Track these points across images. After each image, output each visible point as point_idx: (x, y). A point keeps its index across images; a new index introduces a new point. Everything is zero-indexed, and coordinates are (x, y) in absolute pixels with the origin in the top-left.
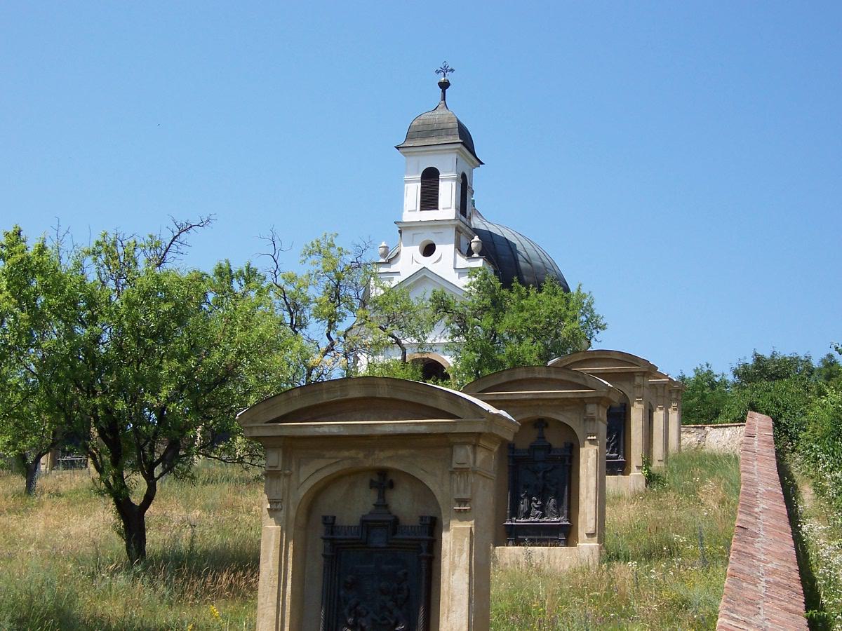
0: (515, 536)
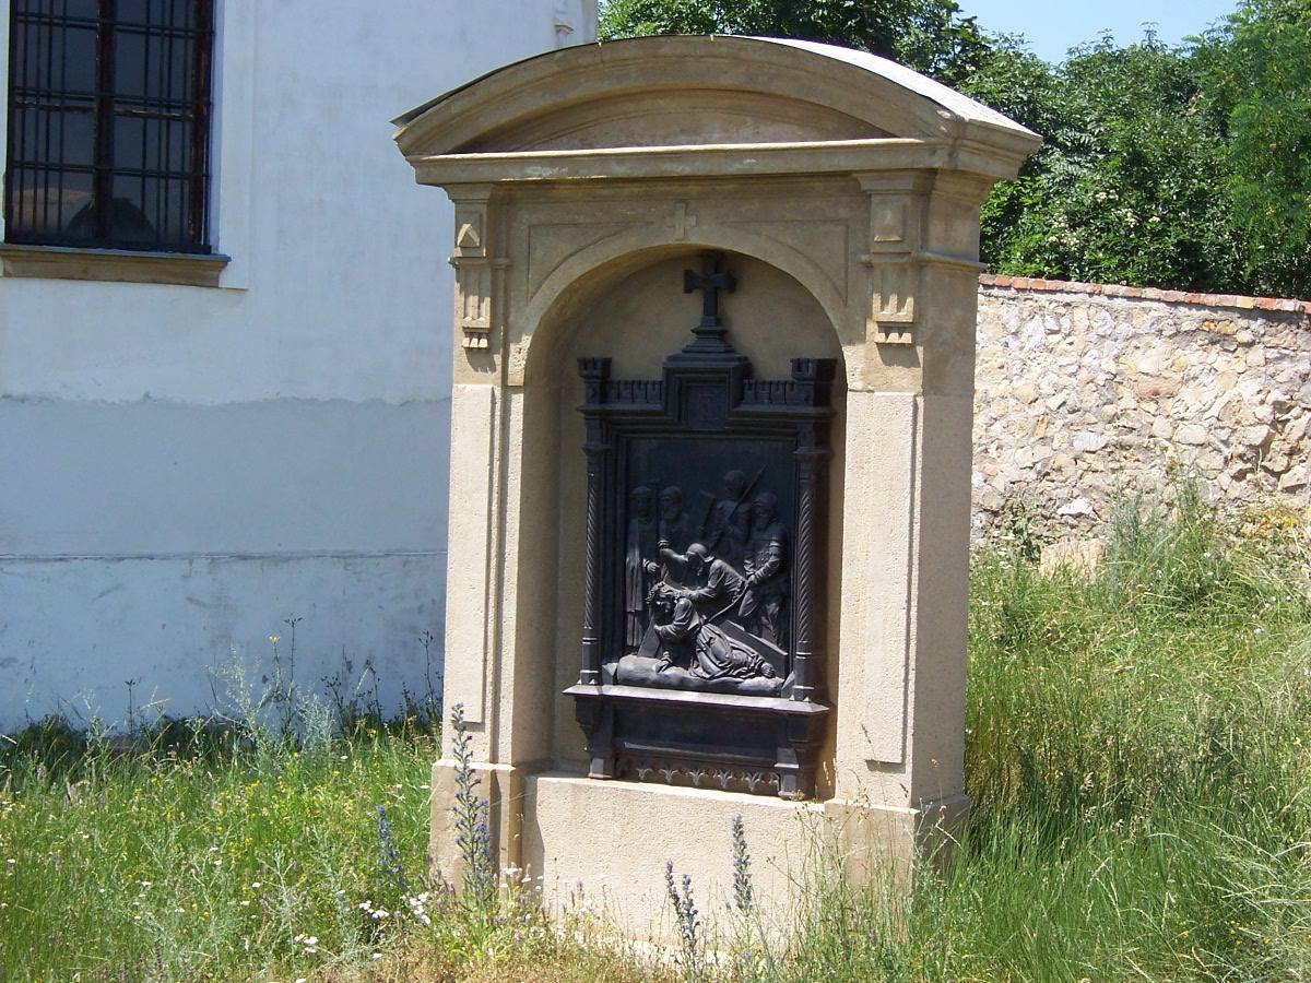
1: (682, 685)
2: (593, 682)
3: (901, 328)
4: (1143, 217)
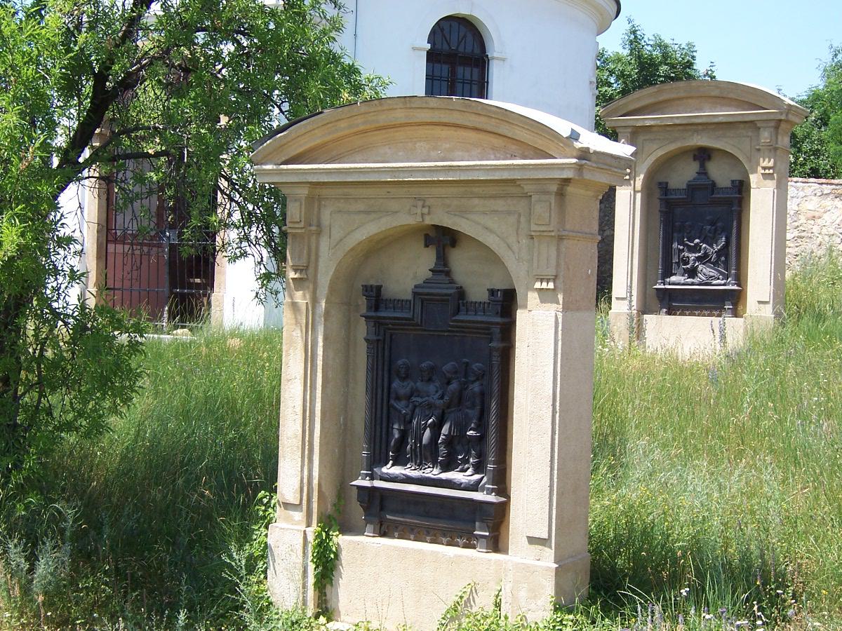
0: (672, 302)
1: (693, 284)
2: (368, 478)
3: (769, 168)
4: (797, 159)
